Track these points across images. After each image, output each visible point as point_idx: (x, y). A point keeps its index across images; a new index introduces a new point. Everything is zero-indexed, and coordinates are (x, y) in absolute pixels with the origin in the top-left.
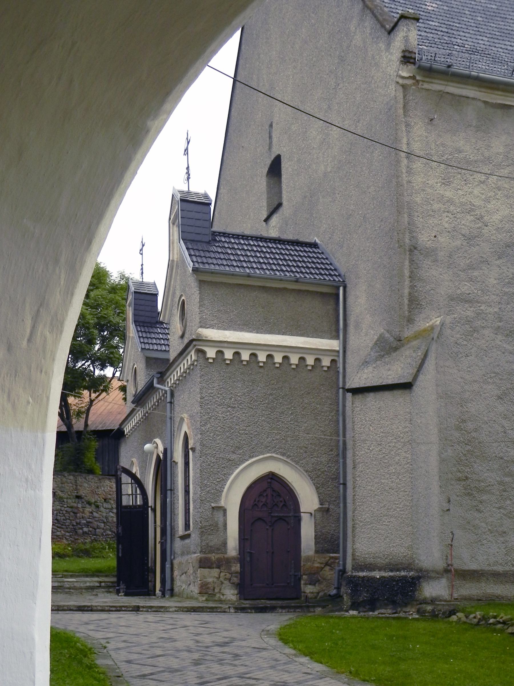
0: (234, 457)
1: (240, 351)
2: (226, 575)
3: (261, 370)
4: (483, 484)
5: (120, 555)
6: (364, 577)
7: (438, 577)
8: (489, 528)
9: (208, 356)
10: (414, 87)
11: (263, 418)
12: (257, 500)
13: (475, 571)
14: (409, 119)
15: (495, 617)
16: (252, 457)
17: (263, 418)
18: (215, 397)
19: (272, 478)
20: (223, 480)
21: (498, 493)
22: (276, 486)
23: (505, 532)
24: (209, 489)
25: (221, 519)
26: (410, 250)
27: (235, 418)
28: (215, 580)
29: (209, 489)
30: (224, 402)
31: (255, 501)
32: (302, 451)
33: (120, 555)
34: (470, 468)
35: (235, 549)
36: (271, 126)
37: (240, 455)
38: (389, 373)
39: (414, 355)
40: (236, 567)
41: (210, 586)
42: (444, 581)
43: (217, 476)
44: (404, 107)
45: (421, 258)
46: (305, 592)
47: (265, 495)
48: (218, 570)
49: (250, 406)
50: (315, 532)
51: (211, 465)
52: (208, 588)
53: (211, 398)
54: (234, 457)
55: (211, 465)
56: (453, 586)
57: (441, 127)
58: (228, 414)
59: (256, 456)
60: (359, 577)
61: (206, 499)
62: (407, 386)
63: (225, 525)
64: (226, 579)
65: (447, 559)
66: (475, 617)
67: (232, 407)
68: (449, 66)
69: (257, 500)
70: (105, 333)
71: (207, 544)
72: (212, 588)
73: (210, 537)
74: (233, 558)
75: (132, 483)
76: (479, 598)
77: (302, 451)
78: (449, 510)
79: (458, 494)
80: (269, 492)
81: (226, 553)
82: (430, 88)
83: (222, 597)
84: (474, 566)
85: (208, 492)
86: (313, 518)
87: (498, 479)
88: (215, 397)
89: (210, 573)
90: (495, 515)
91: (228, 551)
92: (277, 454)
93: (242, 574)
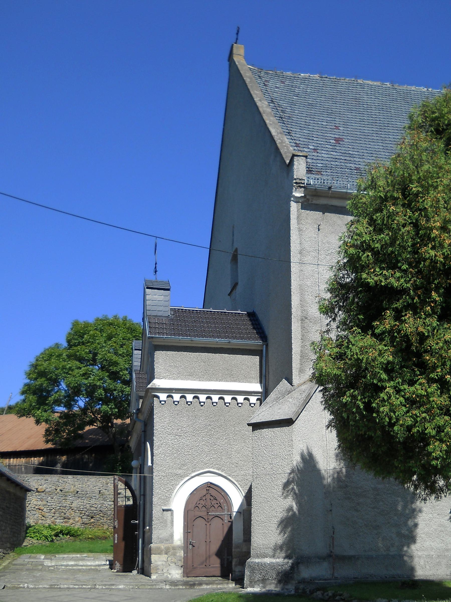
0: (180, 472)
1: (185, 395)
2: (172, 559)
3: (202, 408)
4: (360, 490)
5: (116, 542)
6: (258, 563)
7: (319, 562)
8: (365, 523)
9: (161, 399)
10: (305, 203)
11: (204, 443)
12: (198, 503)
13: (354, 557)
14: (301, 226)
15: (341, 595)
16: (195, 471)
17: (204, 443)
18: (166, 429)
19: (210, 486)
20: (171, 489)
21: (372, 496)
22: (212, 491)
23: (378, 526)
24: (160, 496)
25: (169, 518)
26: (302, 320)
27: (181, 443)
28: (164, 563)
29: (160, 496)
30: (173, 432)
31: (196, 504)
32: (233, 466)
33: (116, 542)
34: (349, 479)
35: (180, 540)
36: (233, 227)
37: (185, 470)
38: (279, 411)
39: (300, 397)
40: (181, 553)
41: (159, 567)
42: (325, 564)
43: (166, 486)
44: (298, 217)
45: (311, 324)
46: (235, 571)
47: (204, 499)
48: (166, 556)
49: (193, 434)
50: (244, 526)
51: (162, 478)
52: (158, 569)
53: (163, 429)
54: (180, 472)
55: (162, 478)
56: (334, 568)
57: (327, 230)
58: (176, 440)
59: (197, 471)
60: (256, 563)
61: (158, 503)
62: (288, 422)
63: (172, 522)
64: (172, 562)
65: (330, 547)
66: (328, 595)
67: (179, 436)
68: (330, 188)
69: (198, 503)
70: (45, 394)
71: (158, 537)
72: (161, 569)
73: (160, 532)
74: (179, 547)
75: (125, 489)
76: (355, 577)
77: (233, 466)
78: (331, 510)
79: (339, 498)
80: (208, 497)
81: (172, 543)
82: (318, 203)
83: (169, 575)
84: (352, 553)
85: (159, 498)
86: (242, 515)
87: (372, 486)
88: (166, 429)
89: (159, 557)
90: (370, 513)
91: (175, 541)
92: (214, 468)
93: (186, 558)
